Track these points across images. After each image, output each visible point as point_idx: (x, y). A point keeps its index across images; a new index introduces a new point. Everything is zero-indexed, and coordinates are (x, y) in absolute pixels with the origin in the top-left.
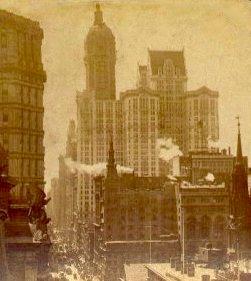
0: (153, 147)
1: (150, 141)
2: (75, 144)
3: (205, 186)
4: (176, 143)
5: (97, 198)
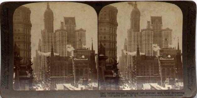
0: (65, 47)
1: (64, 45)
2: (41, 46)
3: (82, 60)
4: (72, 46)
5: (48, 63)
